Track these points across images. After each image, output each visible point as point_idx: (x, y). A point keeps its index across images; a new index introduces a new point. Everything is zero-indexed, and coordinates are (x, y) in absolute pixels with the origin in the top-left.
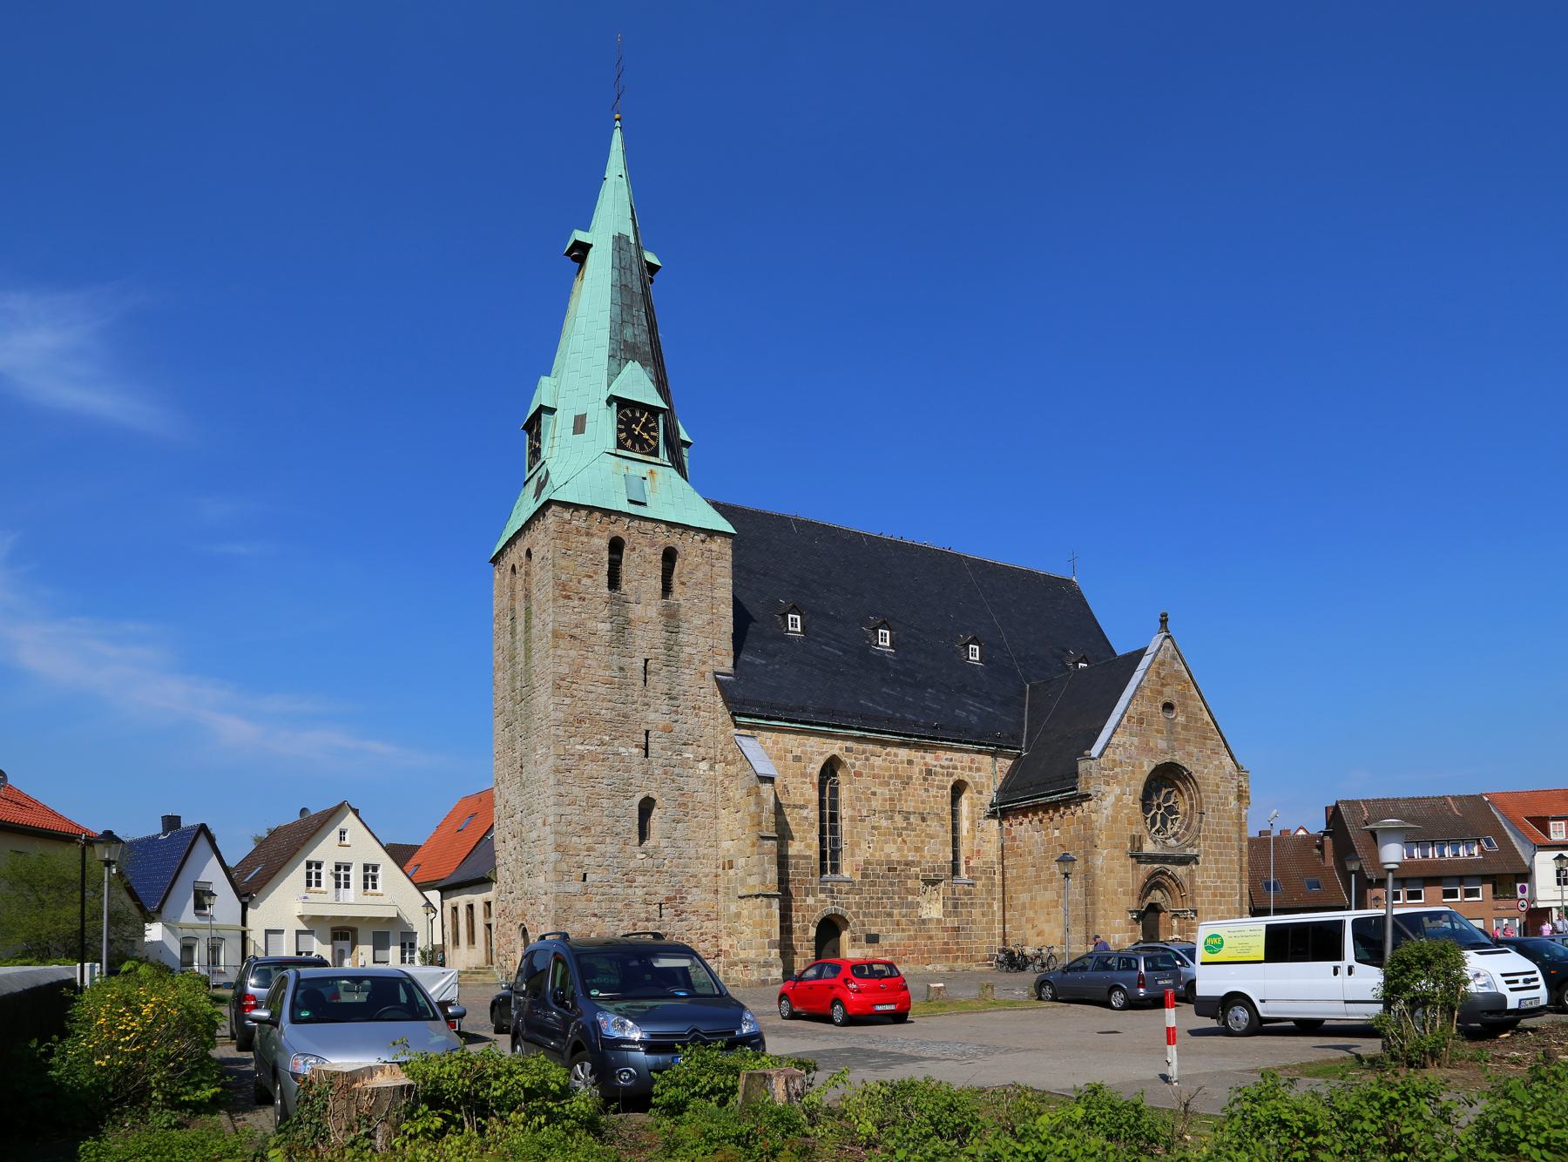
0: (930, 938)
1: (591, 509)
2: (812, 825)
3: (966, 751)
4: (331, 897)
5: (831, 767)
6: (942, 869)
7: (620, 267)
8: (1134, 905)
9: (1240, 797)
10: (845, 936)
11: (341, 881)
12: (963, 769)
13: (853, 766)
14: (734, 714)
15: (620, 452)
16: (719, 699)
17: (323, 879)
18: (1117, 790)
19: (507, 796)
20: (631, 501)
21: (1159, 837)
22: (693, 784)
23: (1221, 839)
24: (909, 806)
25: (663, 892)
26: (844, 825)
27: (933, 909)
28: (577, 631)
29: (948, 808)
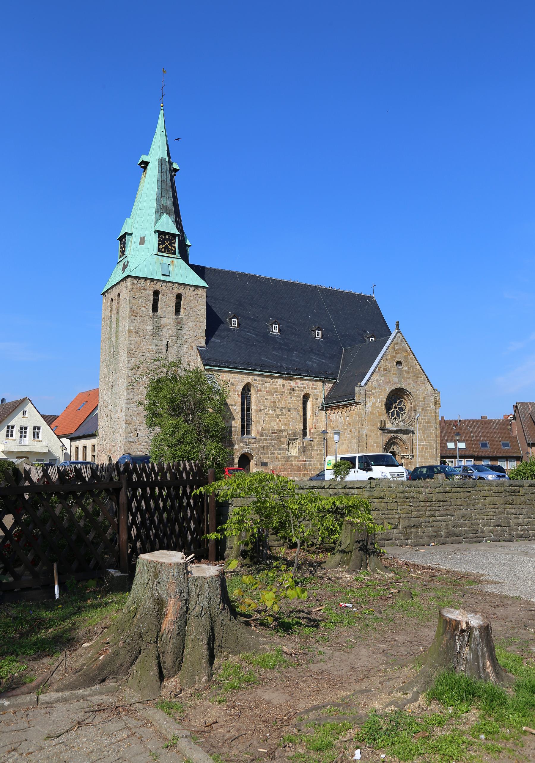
0: (292, 464)
1: (146, 279)
2: (238, 413)
3: (310, 380)
4: (17, 442)
5: (247, 389)
6: (298, 433)
7: (161, 172)
9: (435, 404)
10: (252, 462)
11: (23, 435)
12: (308, 388)
13: (257, 387)
14: (204, 365)
15: (159, 253)
16: (199, 357)
17: (14, 434)
18: (373, 400)
19: (104, 398)
20: (163, 275)
21: (395, 422)
23: (426, 423)
26: (253, 413)
27: (294, 452)
28: (138, 330)
29: (301, 406)
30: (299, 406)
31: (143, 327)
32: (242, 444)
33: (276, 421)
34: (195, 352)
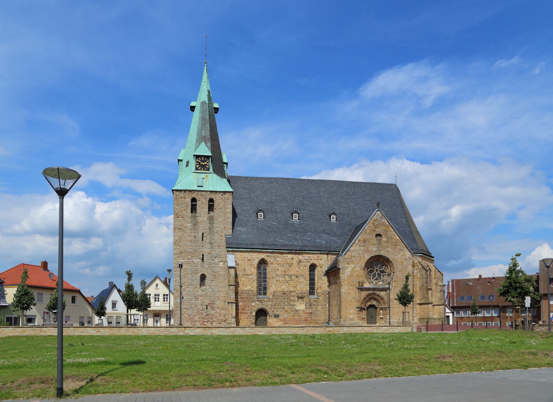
0: (300, 316)
1: (185, 191)
3: (316, 254)
5: (263, 262)
8: (359, 305)
13: (270, 261)
18: (353, 266)
22: (218, 269)
24: (292, 273)
25: (207, 302)
30: (306, 274)
31: (185, 224)
32: (258, 302)
33: (285, 285)
34: (224, 239)
